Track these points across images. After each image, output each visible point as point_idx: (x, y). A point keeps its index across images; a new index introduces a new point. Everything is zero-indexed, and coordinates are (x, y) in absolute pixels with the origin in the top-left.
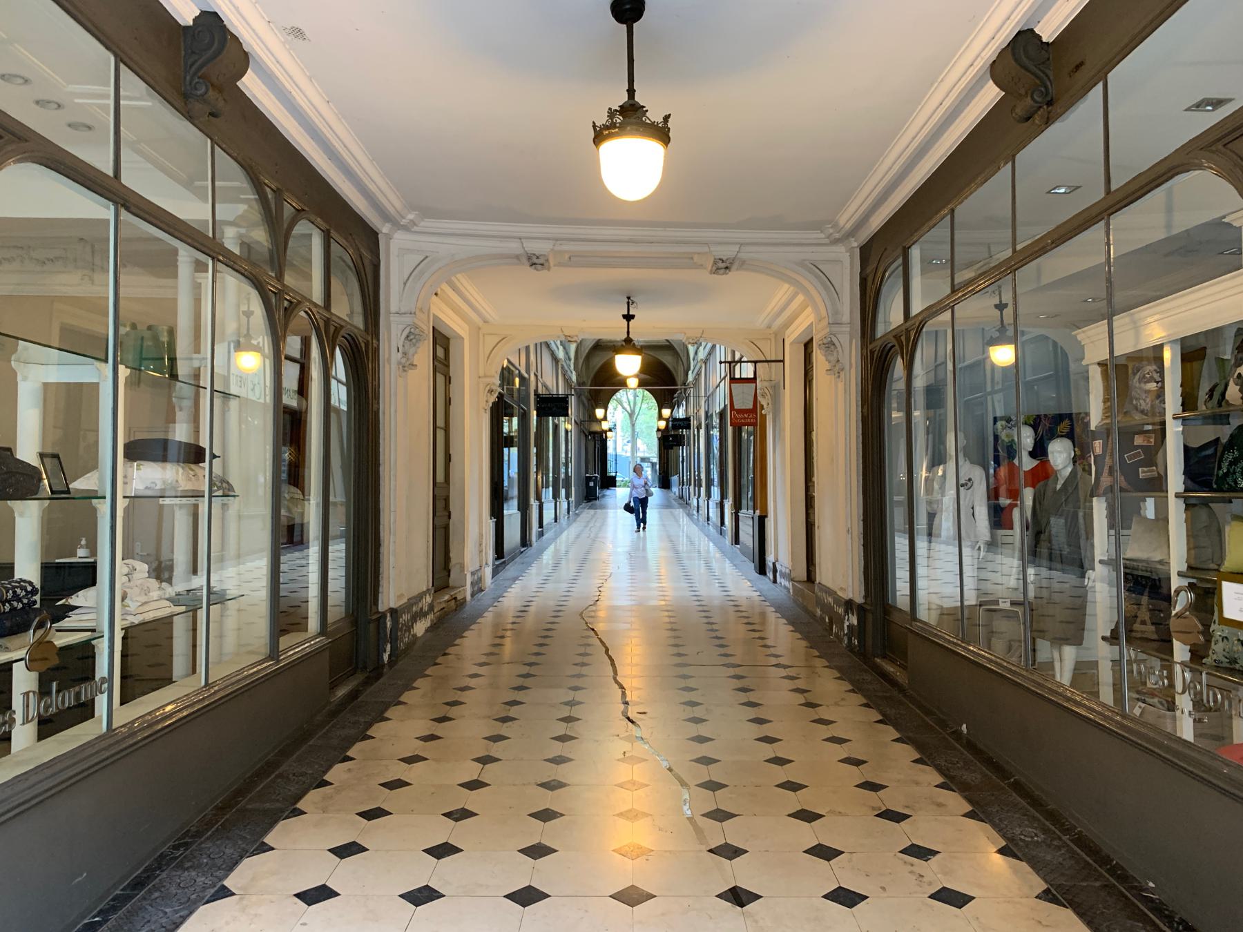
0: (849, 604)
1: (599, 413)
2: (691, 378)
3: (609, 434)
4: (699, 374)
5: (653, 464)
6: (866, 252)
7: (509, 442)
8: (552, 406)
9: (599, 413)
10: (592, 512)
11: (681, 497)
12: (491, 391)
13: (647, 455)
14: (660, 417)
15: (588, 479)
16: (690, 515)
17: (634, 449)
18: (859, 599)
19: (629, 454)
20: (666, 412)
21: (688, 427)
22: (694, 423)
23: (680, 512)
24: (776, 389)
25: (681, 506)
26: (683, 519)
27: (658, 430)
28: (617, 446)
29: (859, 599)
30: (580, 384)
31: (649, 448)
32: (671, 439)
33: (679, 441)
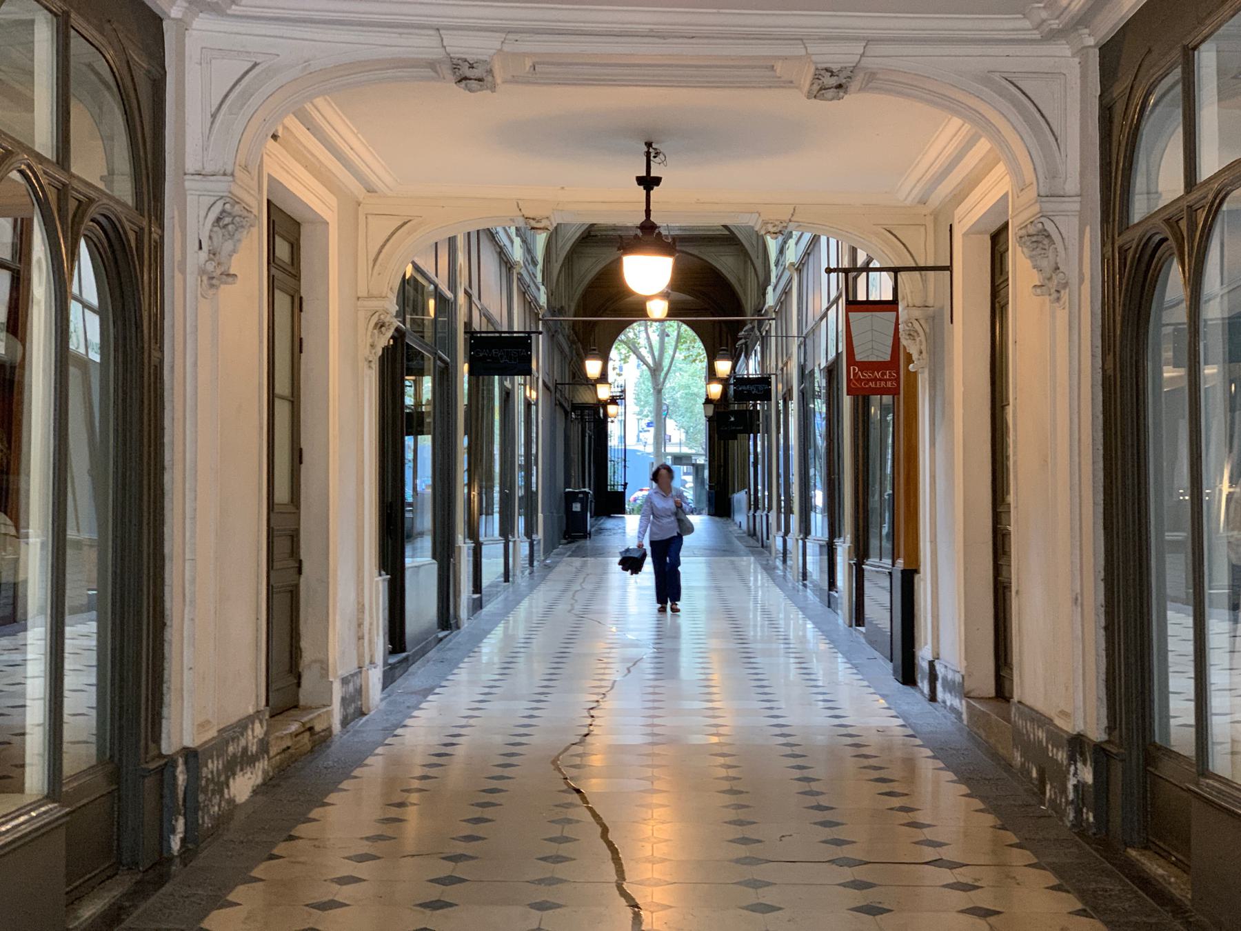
0: (1077, 744)
1: (593, 368)
2: (771, 299)
3: (612, 409)
4: (786, 292)
5: (698, 469)
6: (1111, 56)
7: (415, 423)
8: (499, 354)
9: (593, 368)
10: (577, 561)
11: (753, 534)
12: (380, 326)
13: (685, 450)
14: (712, 375)
15: (570, 498)
16: (769, 569)
17: (661, 439)
18: (1097, 733)
19: (650, 449)
20: (723, 367)
21: (766, 396)
22: (777, 388)
23: (749, 563)
24: (937, 323)
25: (753, 551)
26: (757, 578)
27: (708, 401)
28: (629, 433)
29: (1097, 733)
30: (554, 310)
31: (687, 437)
32: (733, 418)
33: (749, 424)
